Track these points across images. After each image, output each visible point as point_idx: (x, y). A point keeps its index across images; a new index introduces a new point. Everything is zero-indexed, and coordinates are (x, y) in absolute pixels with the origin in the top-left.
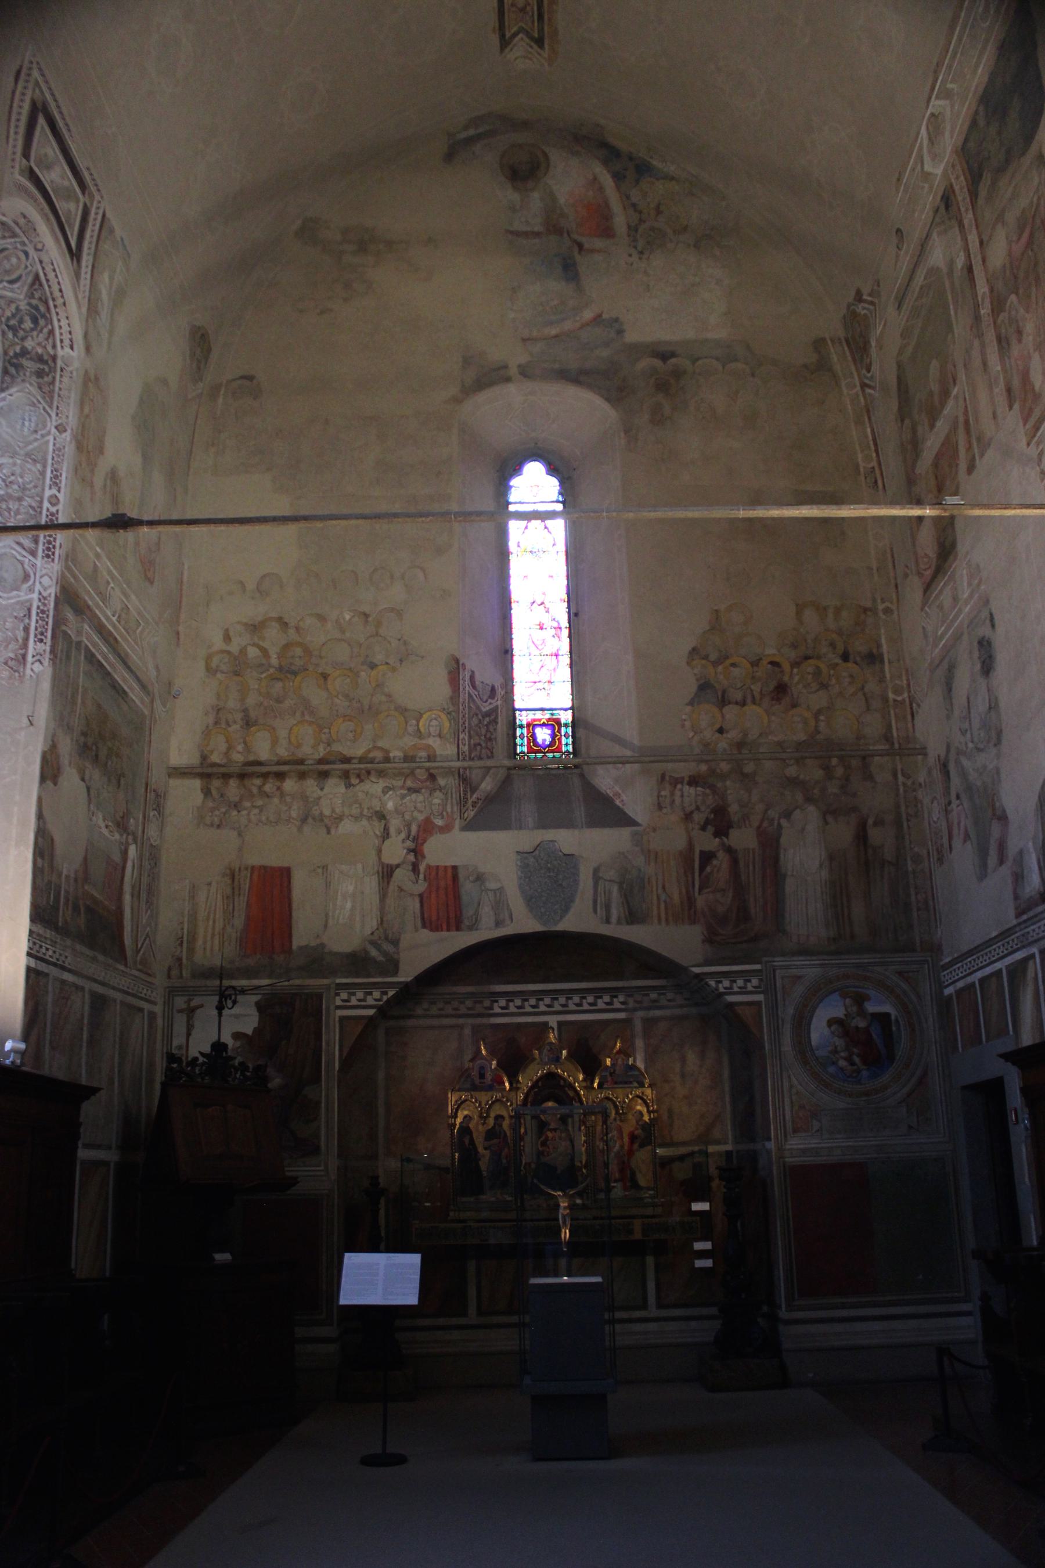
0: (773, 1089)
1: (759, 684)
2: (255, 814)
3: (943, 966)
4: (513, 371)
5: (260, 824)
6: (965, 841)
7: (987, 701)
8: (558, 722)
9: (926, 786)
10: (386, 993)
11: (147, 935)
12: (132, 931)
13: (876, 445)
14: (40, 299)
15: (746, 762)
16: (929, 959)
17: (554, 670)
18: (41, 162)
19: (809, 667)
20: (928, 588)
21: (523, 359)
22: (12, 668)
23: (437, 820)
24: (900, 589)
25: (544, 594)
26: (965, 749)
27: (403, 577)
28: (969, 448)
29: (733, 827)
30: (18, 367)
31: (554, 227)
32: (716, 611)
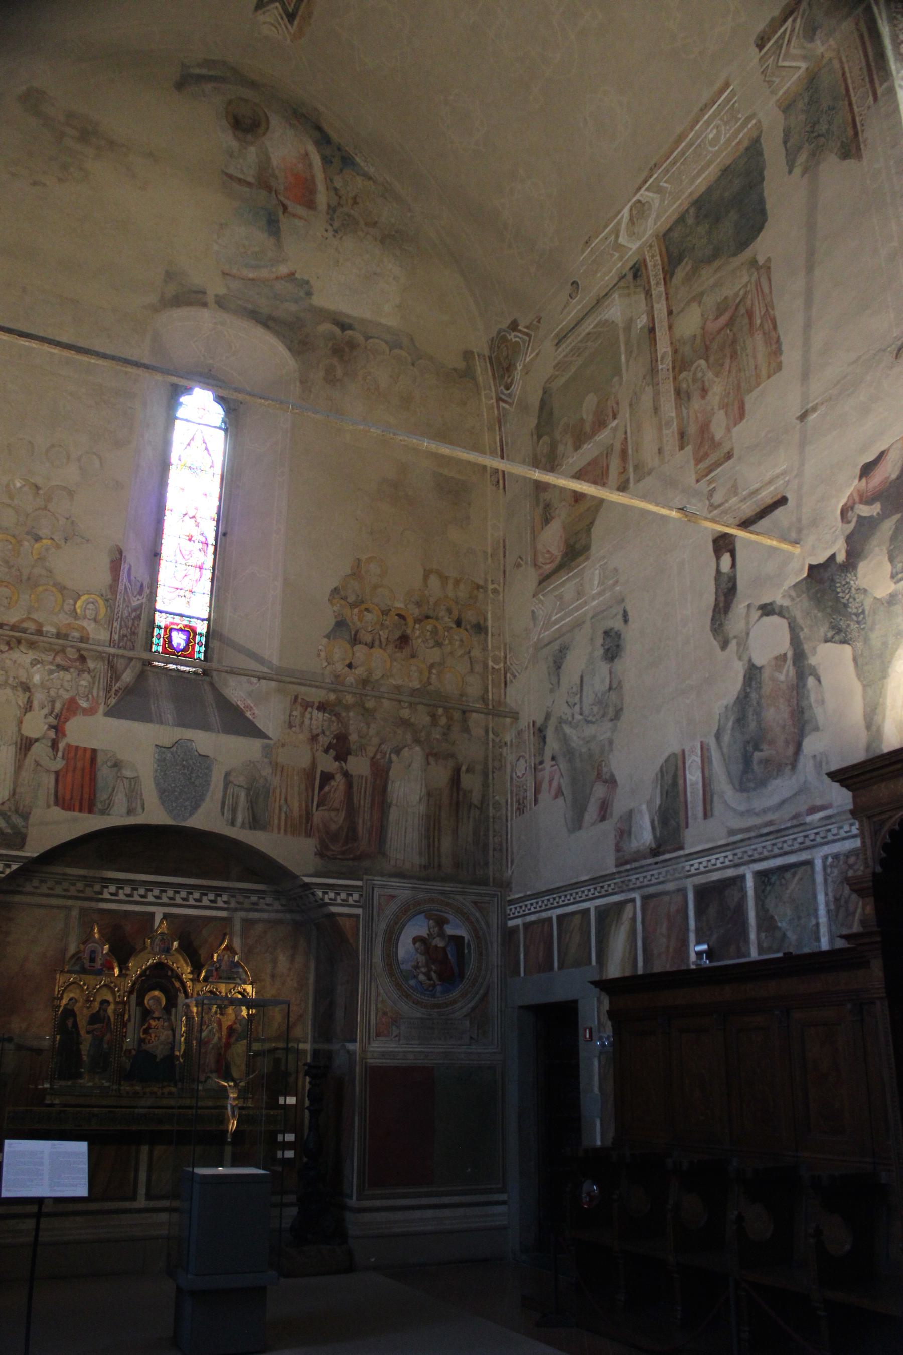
0: (363, 993)
1: (387, 632)
3: (509, 901)
4: (210, 299)
6: (556, 797)
7: (608, 682)
8: (194, 630)
9: (511, 745)
10: (9, 866)
16: (499, 894)
20: (544, 579)
21: (222, 291)
23: (82, 702)
25: (196, 509)
26: (570, 719)
27: (79, 460)
29: (350, 754)
32: (358, 559)
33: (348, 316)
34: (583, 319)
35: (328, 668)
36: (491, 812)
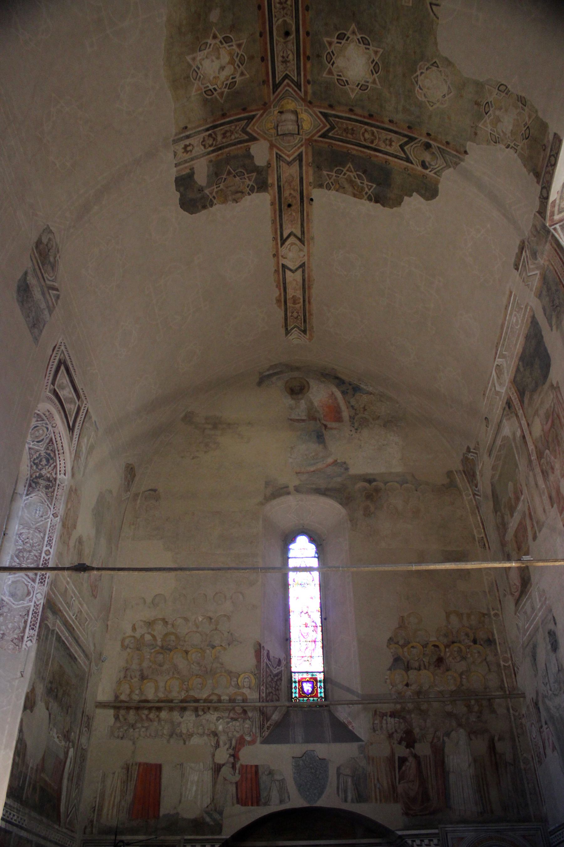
2: (143, 732)
3: (550, 832)
4: (291, 489)
5: (146, 737)
6: (553, 751)
7: (557, 666)
8: (316, 679)
11: (75, 805)
12: (65, 803)
13: (483, 525)
14: (52, 450)
15: (422, 703)
17: (314, 650)
18: (60, 387)
19: (455, 647)
20: (517, 602)
21: (297, 483)
22: (15, 644)
23: (247, 737)
24: (502, 603)
25: (308, 607)
28: (533, 527)
29: (416, 742)
30: (37, 483)
31: (312, 417)
32: (402, 617)
33: (371, 474)
34: (495, 437)
35: (393, 689)
36: (522, 766)
